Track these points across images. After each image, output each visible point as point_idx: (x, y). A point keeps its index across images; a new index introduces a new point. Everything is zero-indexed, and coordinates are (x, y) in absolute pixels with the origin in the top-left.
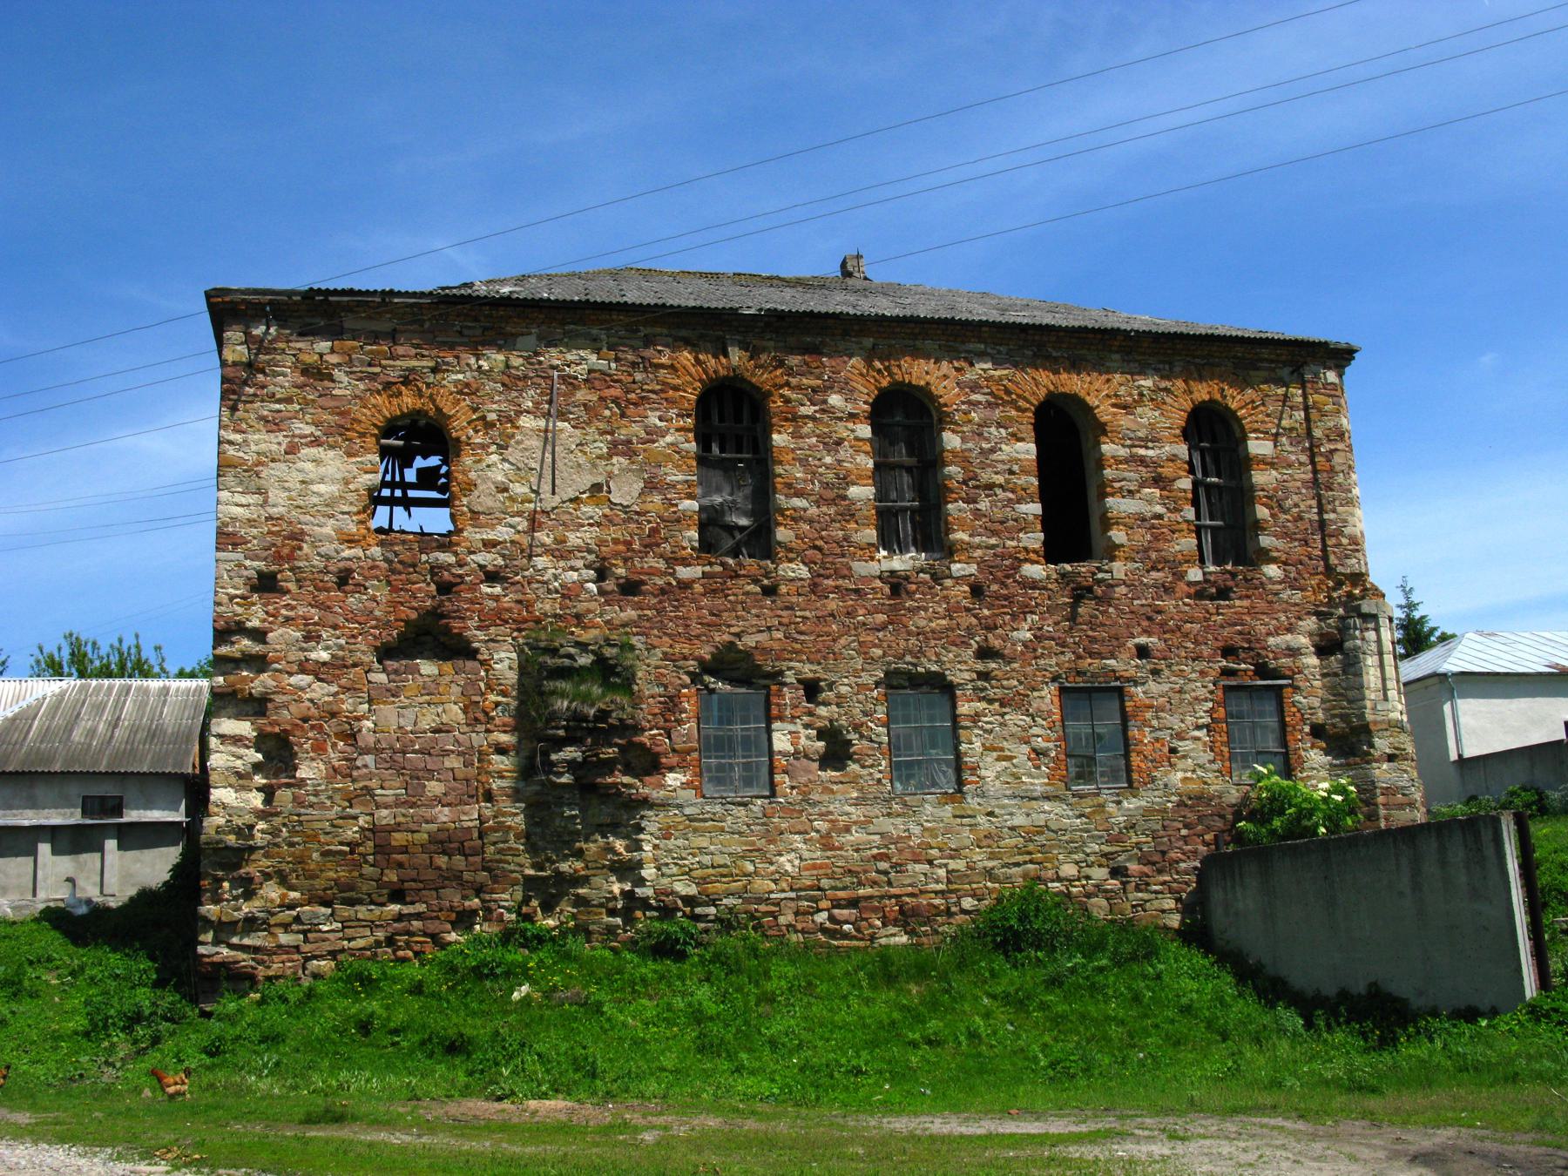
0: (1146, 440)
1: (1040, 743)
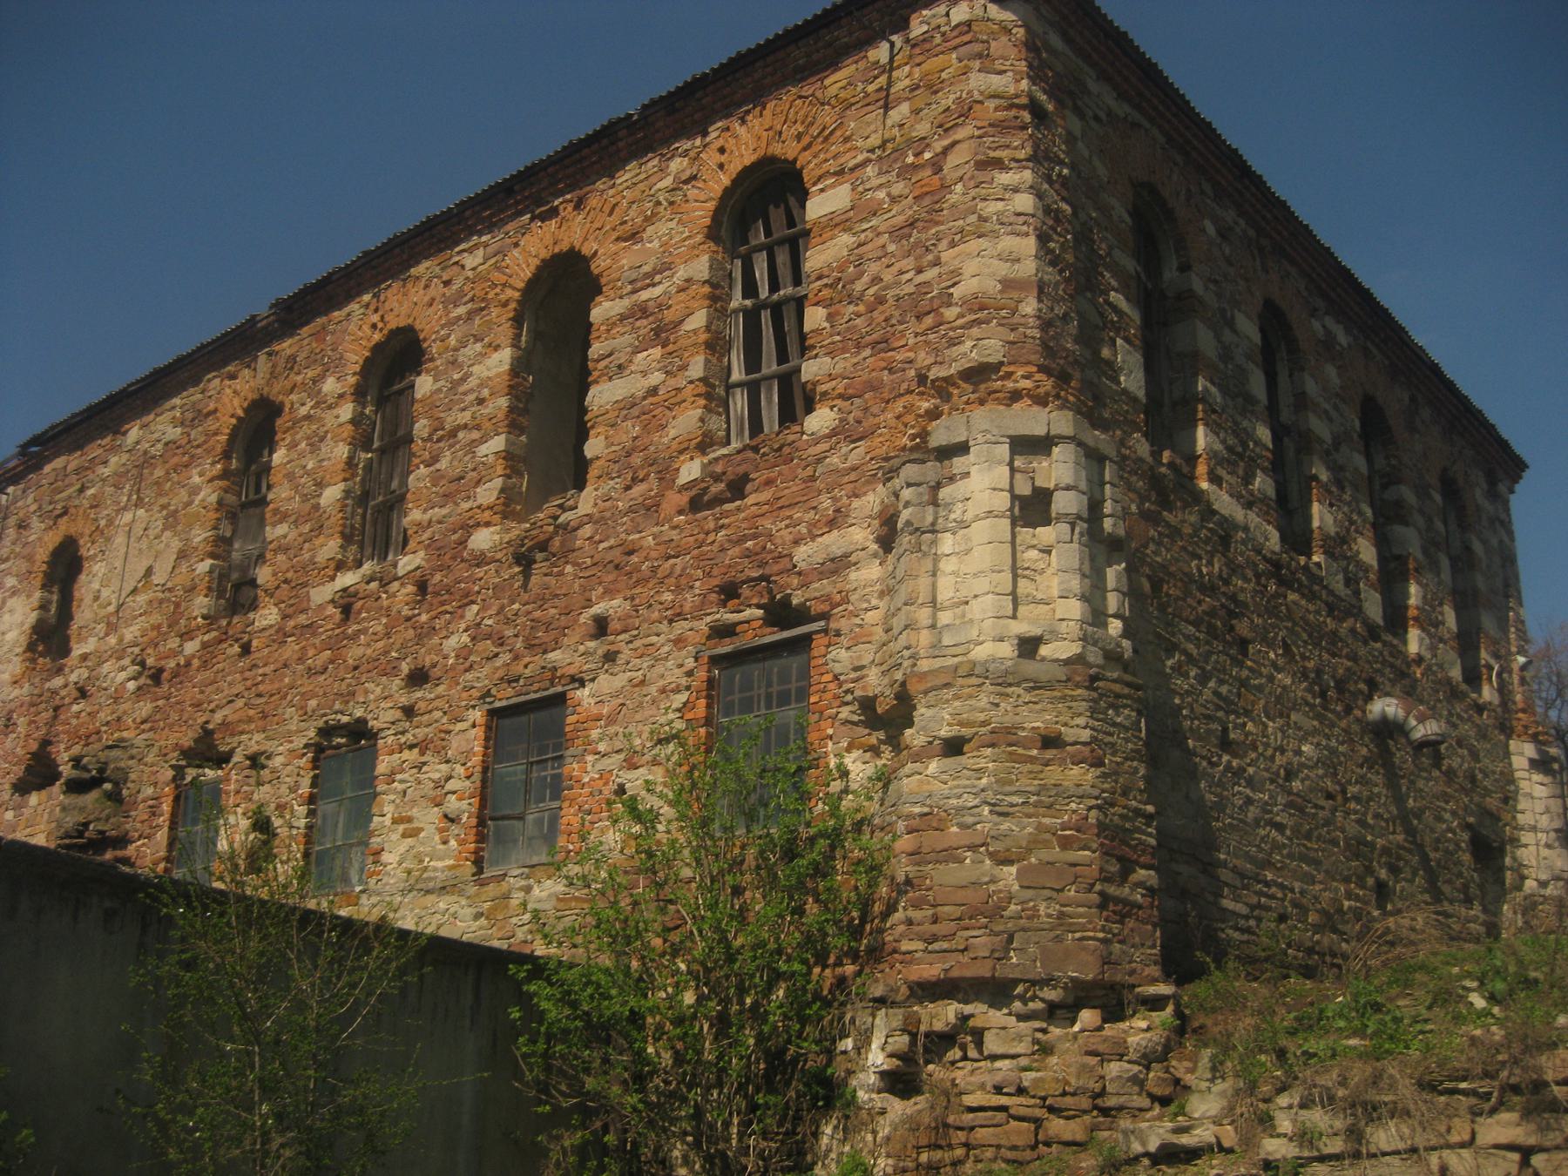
0: (656, 272)
1: (452, 804)
